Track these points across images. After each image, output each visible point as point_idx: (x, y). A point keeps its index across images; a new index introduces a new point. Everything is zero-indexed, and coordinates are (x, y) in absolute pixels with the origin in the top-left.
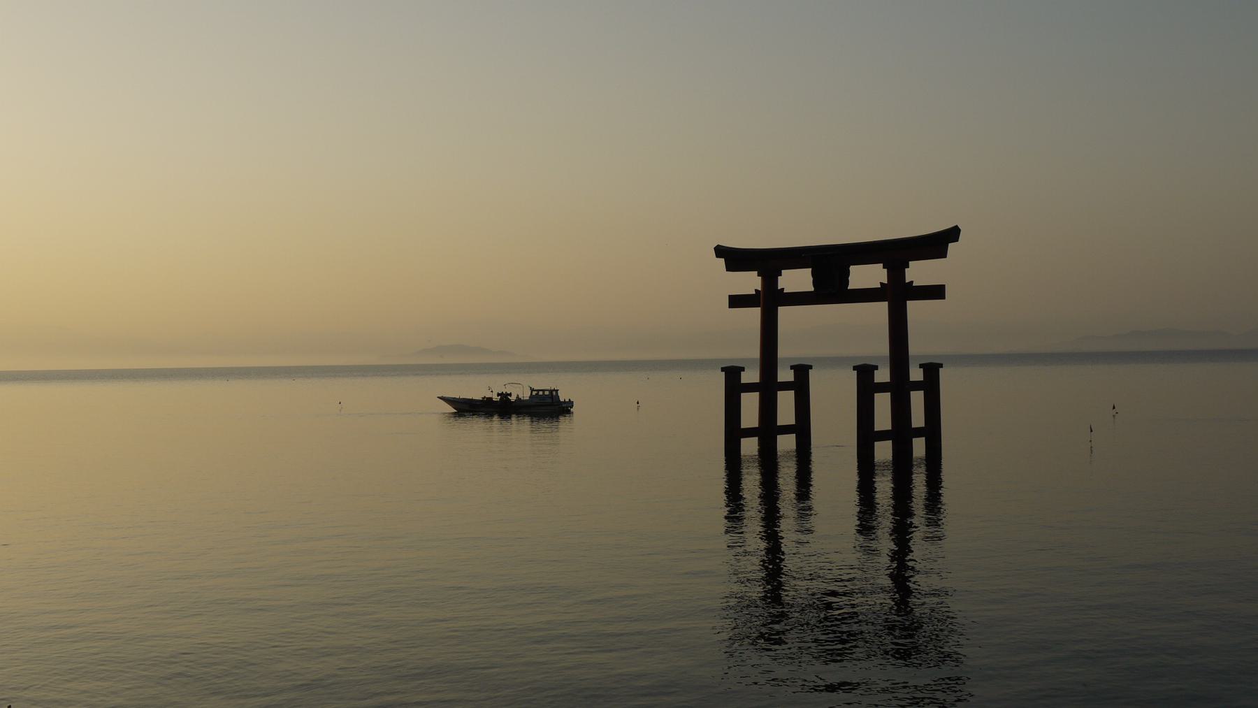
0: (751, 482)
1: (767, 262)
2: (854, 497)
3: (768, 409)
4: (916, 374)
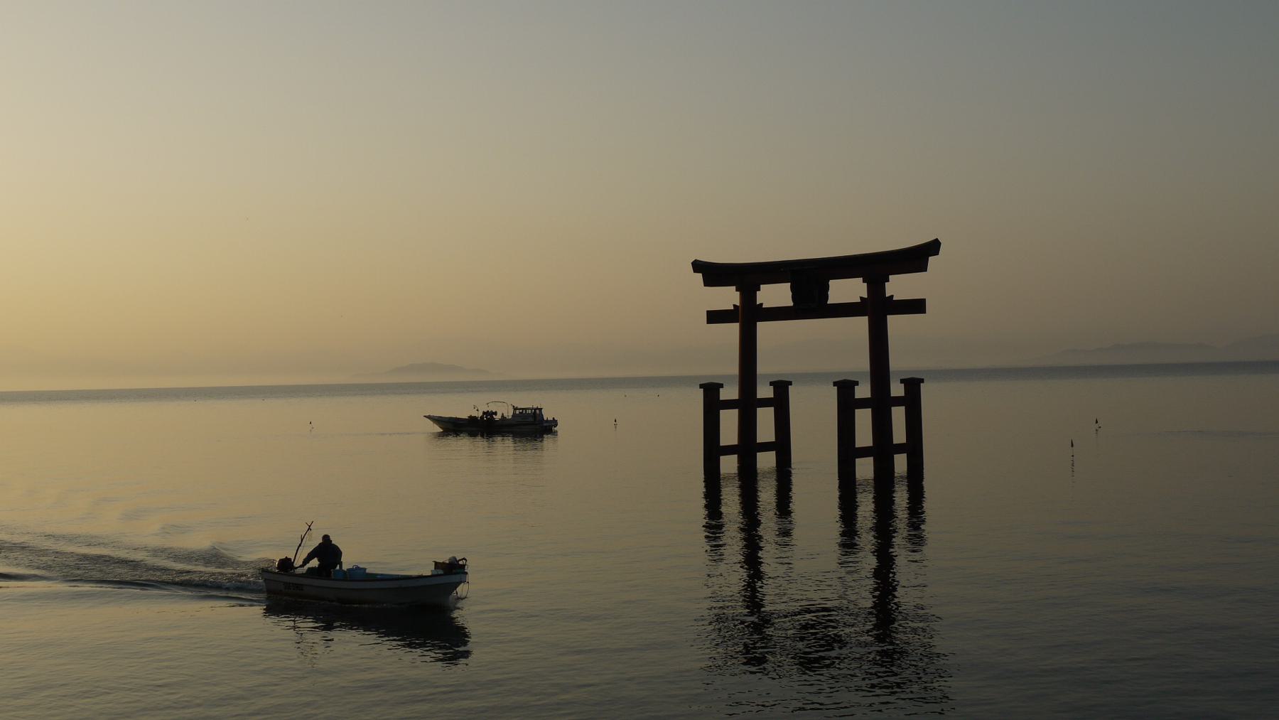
0: (866, 506)
1: (745, 277)
3: (747, 426)
4: (897, 390)
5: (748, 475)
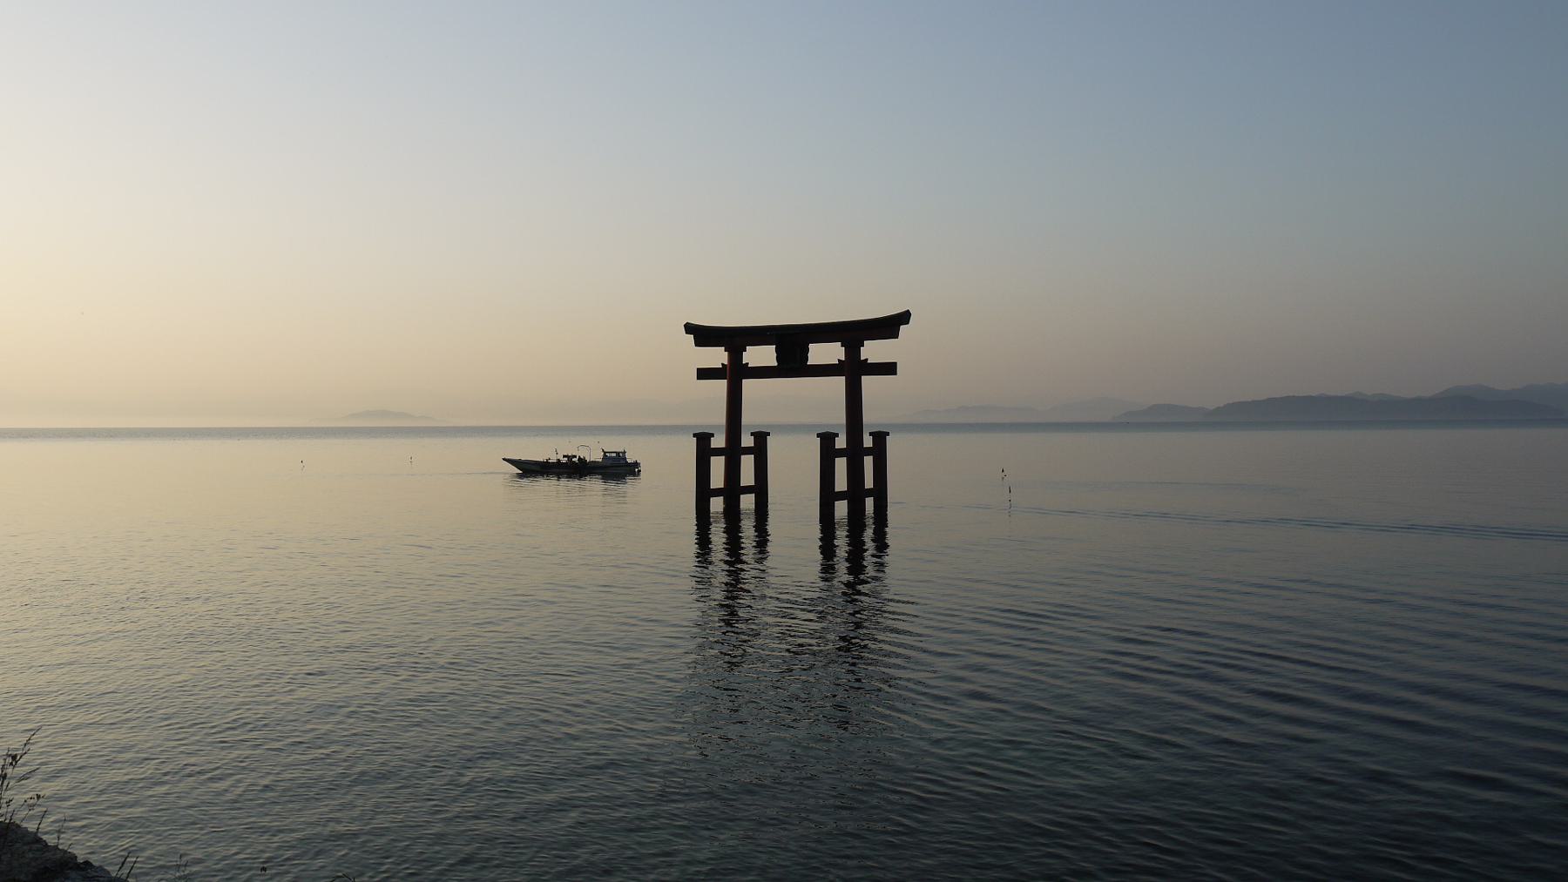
0: (718, 537)
1: (734, 339)
2: (693, 538)
3: (733, 471)
4: (868, 442)
5: (732, 515)
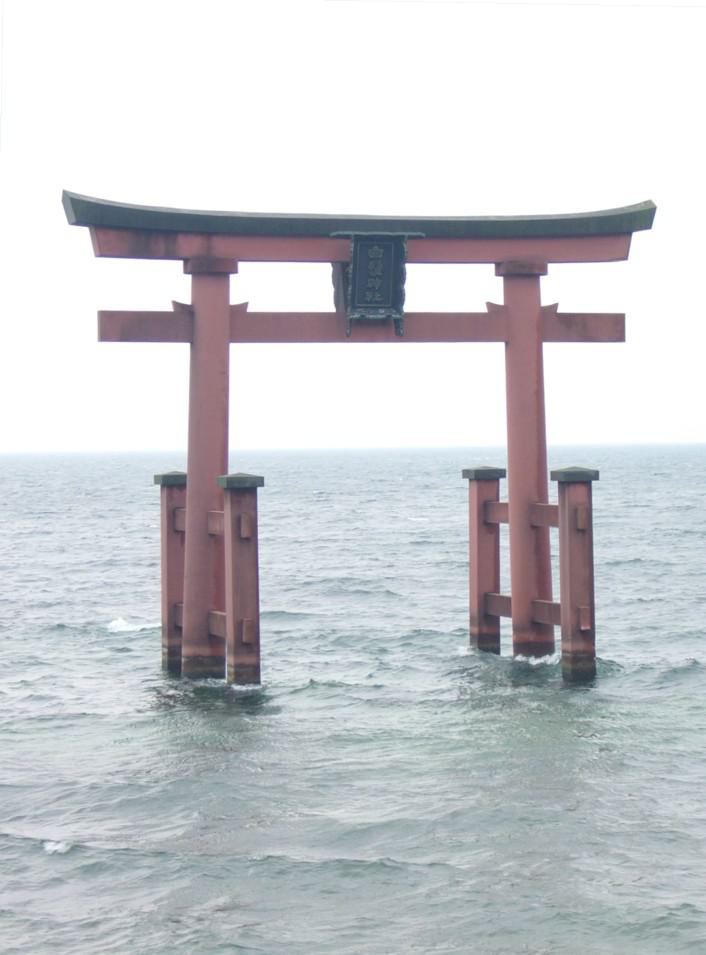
1: (209, 242)
